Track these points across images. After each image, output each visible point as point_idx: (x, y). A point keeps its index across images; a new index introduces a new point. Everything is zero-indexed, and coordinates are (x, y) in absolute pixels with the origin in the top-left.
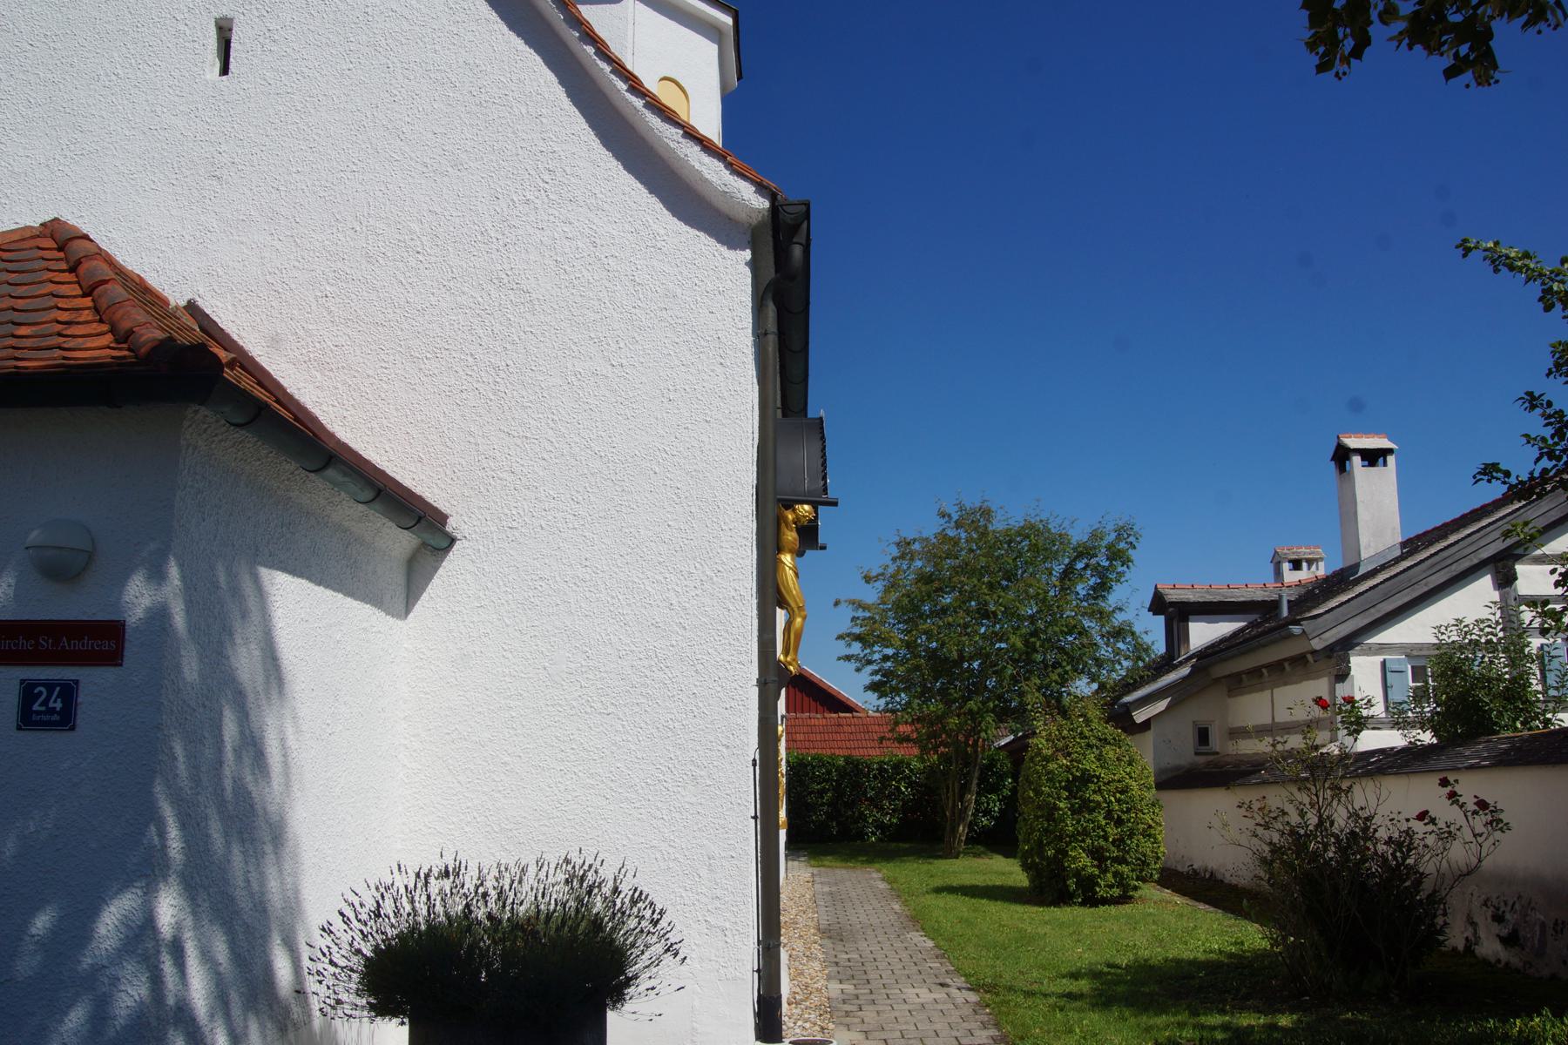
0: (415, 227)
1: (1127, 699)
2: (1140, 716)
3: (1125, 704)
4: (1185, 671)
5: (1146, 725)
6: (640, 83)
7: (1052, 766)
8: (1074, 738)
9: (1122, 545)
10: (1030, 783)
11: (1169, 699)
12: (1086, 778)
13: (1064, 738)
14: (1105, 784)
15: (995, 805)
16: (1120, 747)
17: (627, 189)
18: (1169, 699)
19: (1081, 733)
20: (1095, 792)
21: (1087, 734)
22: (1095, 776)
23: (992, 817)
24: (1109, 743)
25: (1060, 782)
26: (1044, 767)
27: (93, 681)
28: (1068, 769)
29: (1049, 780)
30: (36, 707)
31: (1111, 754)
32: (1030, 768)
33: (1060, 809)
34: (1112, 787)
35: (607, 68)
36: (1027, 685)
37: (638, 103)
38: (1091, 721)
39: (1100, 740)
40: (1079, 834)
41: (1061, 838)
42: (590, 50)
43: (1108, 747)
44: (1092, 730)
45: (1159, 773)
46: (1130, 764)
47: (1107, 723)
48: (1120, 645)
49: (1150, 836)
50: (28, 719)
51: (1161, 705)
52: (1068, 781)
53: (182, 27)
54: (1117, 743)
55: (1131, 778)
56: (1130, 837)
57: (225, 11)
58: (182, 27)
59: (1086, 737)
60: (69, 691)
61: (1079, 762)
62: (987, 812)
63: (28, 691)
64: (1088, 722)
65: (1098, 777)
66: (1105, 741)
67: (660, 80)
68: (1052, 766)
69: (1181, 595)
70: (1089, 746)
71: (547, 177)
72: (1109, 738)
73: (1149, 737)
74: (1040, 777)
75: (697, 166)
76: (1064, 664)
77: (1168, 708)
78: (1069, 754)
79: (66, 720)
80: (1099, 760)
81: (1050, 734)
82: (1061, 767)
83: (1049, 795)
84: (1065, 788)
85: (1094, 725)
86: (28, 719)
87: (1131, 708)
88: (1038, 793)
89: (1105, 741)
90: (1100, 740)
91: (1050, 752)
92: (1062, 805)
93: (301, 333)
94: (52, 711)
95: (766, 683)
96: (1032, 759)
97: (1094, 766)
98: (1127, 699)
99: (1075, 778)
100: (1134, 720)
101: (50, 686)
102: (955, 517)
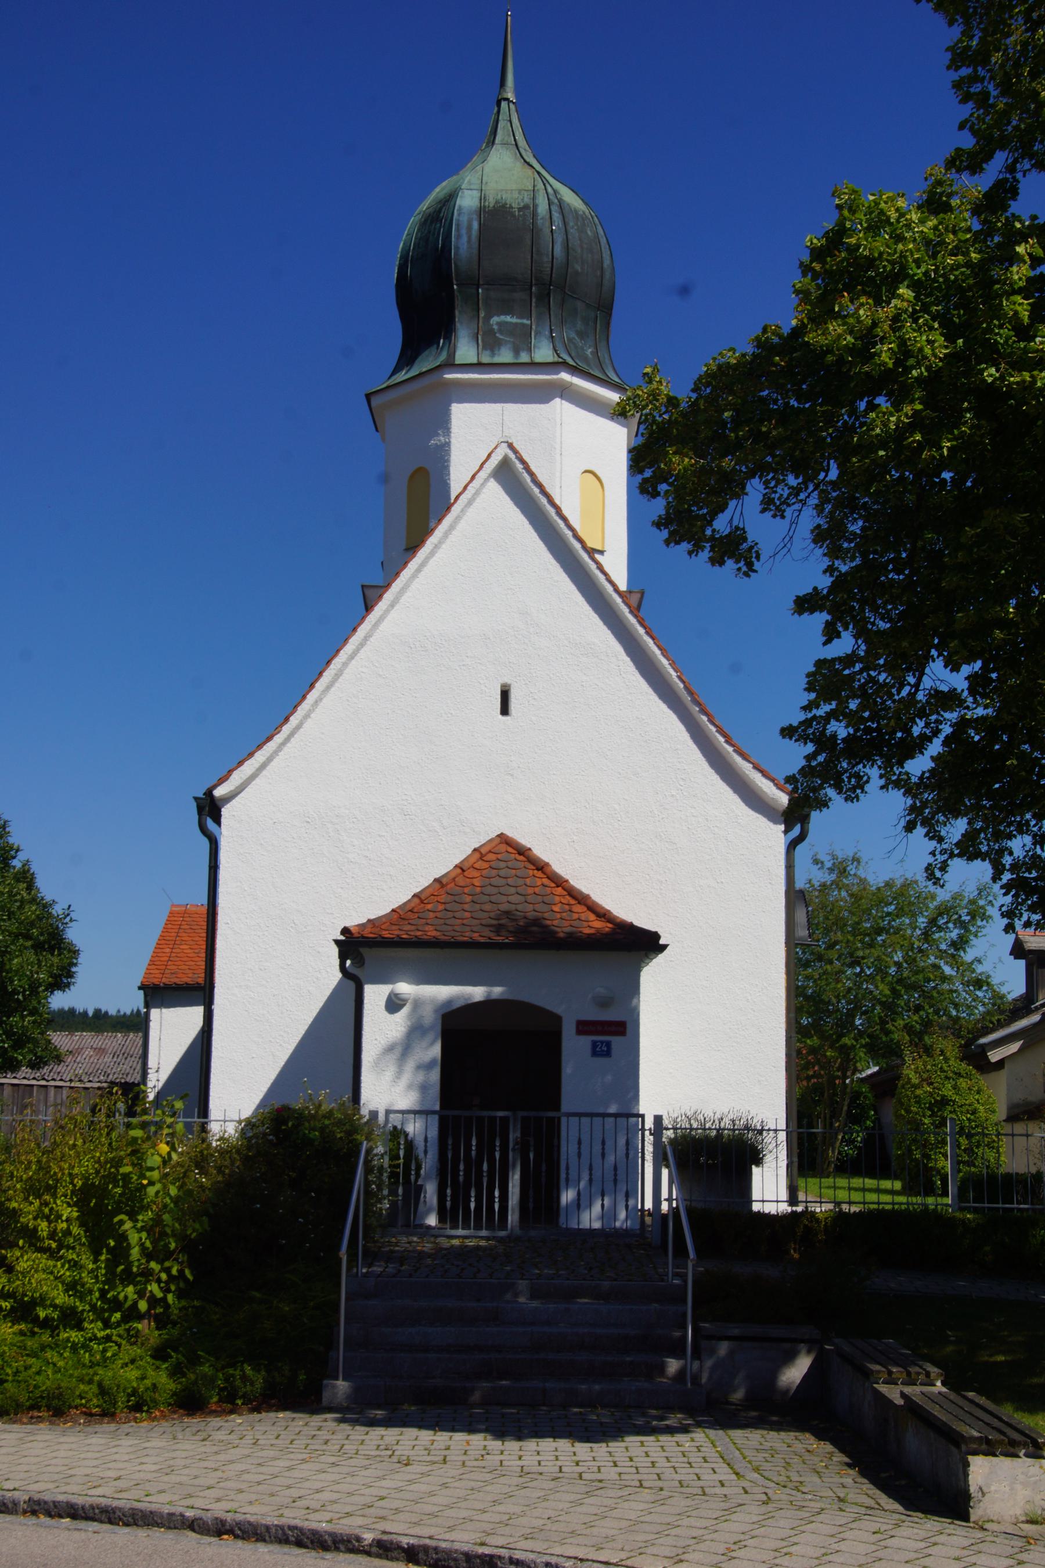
0: (617, 807)
1: (983, 1041)
2: (994, 1056)
3: (983, 1046)
4: (1036, 1018)
5: (1001, 1064)
6: (731, 739)
7: (918, 1092)
8: (936, 1072)
9: (981, 903)
10: (902, 1104)
11: (1022, 1042)
12: (944, 1102)
13: (928, 1071)
14: (959, 1107)
15: (858, 1136)
16: (971, 1080)
17: (722, 791)
18: (1022, 1042)
19: (941, 1068)
20: (951, 1112)
21: (946, 1069)
22: (951, 1100)
23: (855, 1147)
24: (962, 1077)
25: (925, 1104)
26: (913, 1092)
27: (616, 1041)
28: (931, 1094)
29: (916, 1102)
30: (598, 1049)
31: (964, 1085)
32: (902, 1093)
33: (925, 1124)
34: (964, 1109)
35: (714, 729)
36: (893, 1025)
37: (730, 749)
38: (949, 1059)
39: (956, 1074)
40: (939, 1142)
41: (924, 1146)
42: (705, 718)
43: (961, 1080)
44: (949, 1066)
45: (1011, 1108)
46: (978, 1092)
47: (961, 1061)
48: (980, 994)
49: (993, 1148)
50: (595, 1053)
51: (1014, 1047)
52: (930, 1103)
53: (484, 688)
54: (969, 1076)
55: (979, 1103)
56: (977, 1147)
57: (506, 680)
58: (484, 688)
59: (945, 1071)
60: (608, 1044)
61: (939, 1089)
62: (851, 1142)
63: (594, 1044)
64: (946, 1060)
65: (954, 1101)
66: (959, 1075)
67: (586, 471)
68: (918, 1092)
69: (1040, 943)
70: (947, 1078)
71: (682, 783)
72: (963, 1072)
73: (1001, 1078)
74: (909, 1100)
75: (760, 784)
76: (927, 1007)
77: (1020, 1050)
78: (932, 1084)
79: (608, 1053)
80: (954, 1089)
81: (917, 1068)
82: (925, 1093)
83: (916, 1113)
84: (929, 1109)
85: (951, 1062)
86: (595, 1053)
87: (987, 1049)
88: (908, 1111)
89: (959, 1075)
90: (956, 1074)
91: (917, 1081)
92: (926, 1121)
93: (561, 860)
94: (603, 1051)
95: (791, 1037)
96: (903, 1087)
97: (950, 1093)
98: (983, 1041)
99: (936, 1101)
100: (989, 1060)
101: (602, 1042)
102: (828, 865)
